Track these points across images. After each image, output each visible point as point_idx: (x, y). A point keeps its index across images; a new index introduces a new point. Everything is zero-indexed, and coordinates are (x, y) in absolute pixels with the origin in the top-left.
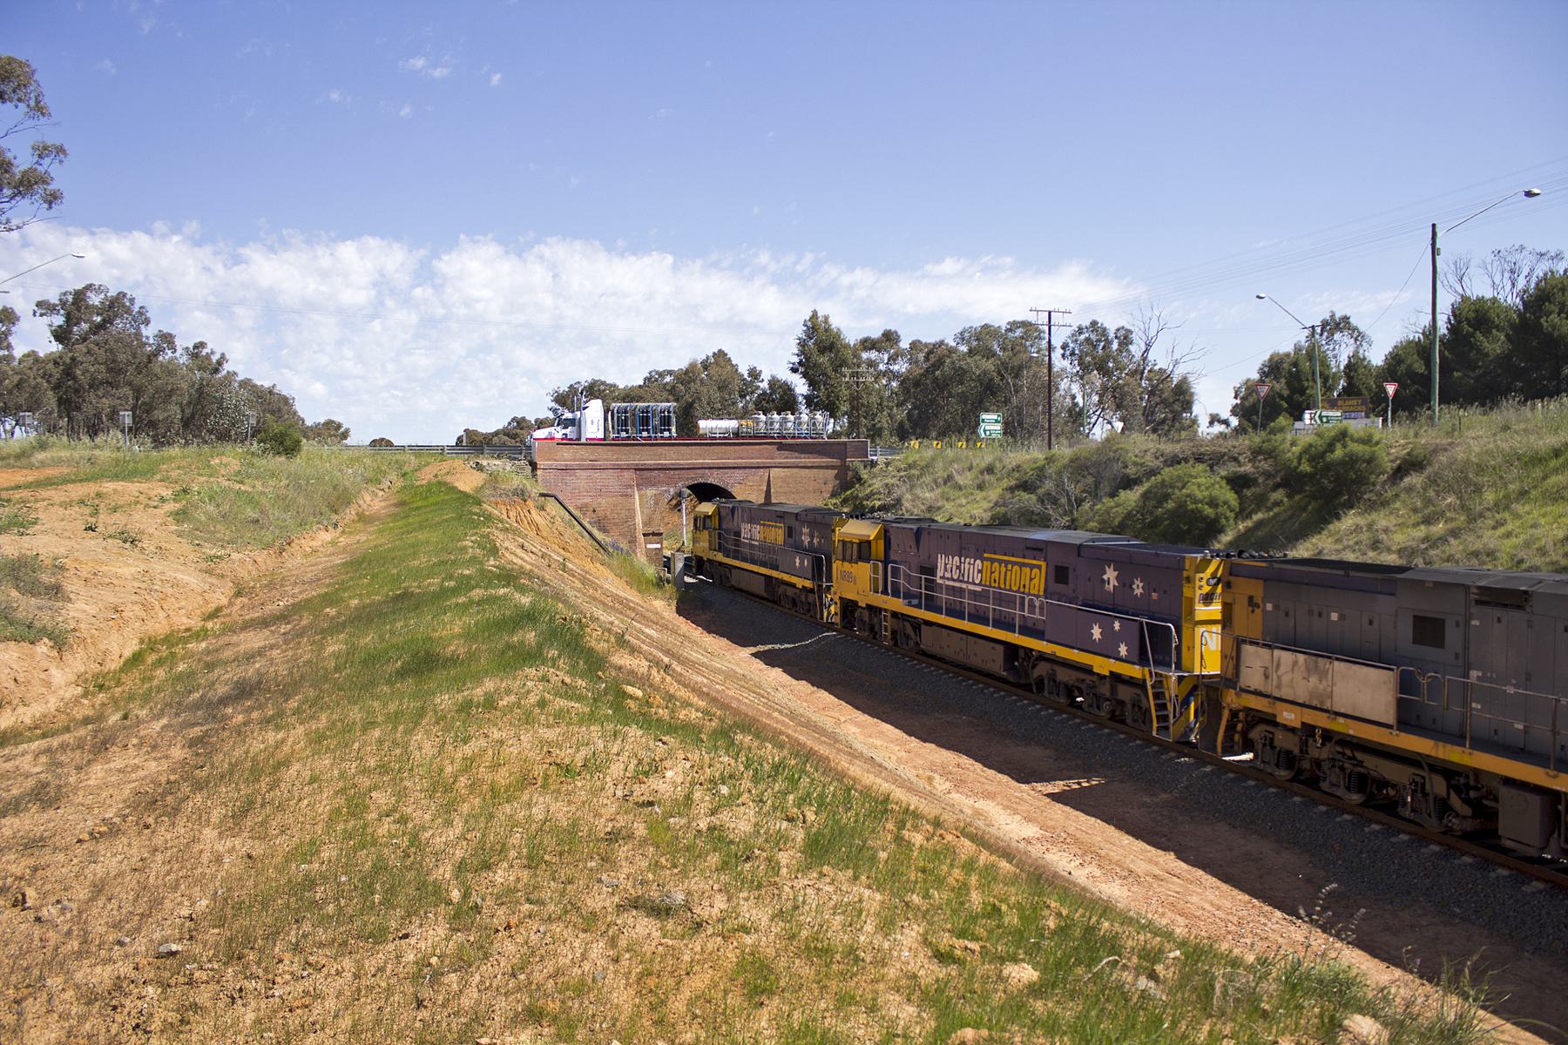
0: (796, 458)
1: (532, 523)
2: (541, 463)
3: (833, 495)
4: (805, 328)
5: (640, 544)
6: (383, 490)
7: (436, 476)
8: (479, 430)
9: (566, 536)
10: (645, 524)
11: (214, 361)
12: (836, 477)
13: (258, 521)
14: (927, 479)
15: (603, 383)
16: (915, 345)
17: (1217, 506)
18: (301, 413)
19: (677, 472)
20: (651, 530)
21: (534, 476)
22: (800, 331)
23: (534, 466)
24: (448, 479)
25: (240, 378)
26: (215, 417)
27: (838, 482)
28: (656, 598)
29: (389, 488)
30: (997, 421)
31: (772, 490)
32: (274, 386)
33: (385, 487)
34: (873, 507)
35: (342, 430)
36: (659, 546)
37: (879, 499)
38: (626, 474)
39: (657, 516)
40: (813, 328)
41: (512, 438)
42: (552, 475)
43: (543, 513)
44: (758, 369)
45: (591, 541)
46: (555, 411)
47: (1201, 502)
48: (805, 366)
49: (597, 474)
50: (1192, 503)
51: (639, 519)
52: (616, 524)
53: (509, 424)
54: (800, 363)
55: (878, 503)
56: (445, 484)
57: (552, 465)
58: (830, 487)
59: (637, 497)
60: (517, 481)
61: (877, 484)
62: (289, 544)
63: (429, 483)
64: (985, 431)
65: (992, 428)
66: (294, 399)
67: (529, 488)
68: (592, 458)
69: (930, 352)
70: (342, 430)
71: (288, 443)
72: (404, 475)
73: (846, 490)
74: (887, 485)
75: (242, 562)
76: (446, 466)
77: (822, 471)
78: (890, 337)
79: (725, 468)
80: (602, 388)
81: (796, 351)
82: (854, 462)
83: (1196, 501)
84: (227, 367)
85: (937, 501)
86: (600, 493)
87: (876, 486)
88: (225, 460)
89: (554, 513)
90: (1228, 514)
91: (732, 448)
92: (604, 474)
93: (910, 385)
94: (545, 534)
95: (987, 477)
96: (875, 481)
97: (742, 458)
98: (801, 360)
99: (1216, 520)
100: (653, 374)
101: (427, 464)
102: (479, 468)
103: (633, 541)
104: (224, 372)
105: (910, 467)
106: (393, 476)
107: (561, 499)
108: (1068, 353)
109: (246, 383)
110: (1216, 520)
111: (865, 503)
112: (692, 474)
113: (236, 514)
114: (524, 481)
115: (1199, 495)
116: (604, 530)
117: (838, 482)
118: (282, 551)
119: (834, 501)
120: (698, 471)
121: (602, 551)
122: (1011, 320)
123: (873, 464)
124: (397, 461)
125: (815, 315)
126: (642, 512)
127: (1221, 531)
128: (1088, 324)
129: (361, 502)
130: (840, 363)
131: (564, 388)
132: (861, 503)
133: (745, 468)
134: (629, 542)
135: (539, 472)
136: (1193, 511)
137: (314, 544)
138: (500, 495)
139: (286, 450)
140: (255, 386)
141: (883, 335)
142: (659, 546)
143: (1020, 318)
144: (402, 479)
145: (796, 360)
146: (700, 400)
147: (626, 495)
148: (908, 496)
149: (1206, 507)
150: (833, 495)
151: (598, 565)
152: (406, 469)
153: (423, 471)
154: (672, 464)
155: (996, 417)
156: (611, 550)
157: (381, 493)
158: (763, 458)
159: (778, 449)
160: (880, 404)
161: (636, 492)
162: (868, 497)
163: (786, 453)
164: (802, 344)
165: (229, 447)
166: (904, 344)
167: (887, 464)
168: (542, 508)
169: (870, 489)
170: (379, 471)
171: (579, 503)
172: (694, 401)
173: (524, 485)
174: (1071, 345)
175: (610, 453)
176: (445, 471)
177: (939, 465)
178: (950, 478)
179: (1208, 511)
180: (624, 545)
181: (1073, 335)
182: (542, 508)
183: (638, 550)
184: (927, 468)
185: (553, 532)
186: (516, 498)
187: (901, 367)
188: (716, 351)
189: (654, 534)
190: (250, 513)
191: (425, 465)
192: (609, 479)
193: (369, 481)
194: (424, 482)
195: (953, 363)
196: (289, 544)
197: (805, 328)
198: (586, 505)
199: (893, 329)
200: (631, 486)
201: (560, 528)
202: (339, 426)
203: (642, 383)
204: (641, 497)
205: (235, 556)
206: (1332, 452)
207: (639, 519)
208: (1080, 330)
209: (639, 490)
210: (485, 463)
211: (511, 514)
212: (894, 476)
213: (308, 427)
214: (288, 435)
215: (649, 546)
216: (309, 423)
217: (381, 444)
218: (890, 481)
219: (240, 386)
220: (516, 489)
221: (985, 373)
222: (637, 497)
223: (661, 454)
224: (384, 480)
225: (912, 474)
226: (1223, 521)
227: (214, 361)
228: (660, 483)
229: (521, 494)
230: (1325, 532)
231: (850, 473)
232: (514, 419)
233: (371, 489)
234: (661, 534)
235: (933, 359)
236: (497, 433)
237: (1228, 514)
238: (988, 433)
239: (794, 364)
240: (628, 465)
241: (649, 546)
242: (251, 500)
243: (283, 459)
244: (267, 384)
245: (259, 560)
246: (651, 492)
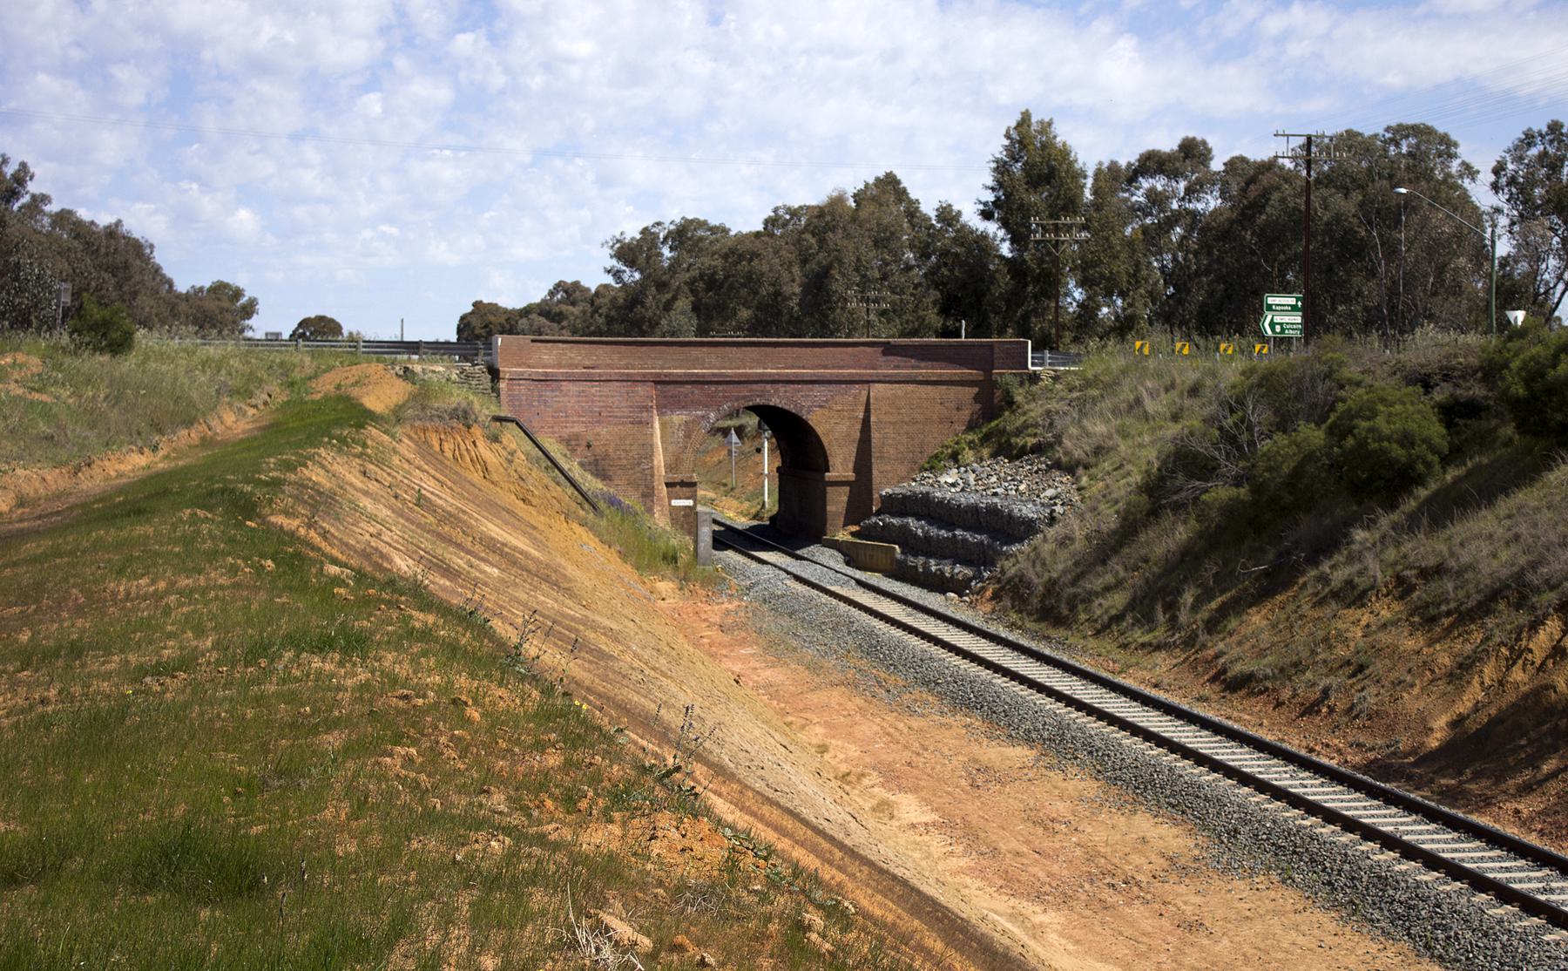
0: (913, 367)
1: (478, 461)
2: (506, 370)
3: (971, 427)
4: (1007, 142)
5: (660, 499)
6: (255, 406)
7: (338, 387)
8: (500, 304)
9: (530, 481)
10: (670, 468)
11: (8, 176)
12: (976, 398)
13: (52, 437)
14: (1107, 404)
15: (702, 224)
16: (1235, 165)
17: (1413, 444)
18: (168, 271)
19: (720, 388)
20: (678, 477)
21: (495, 389)
22: (997, 146)
23: (494, 373)
24: (355, 392)
25: (53, 208)
26: (8, 293)
27: (978, 406)
28: (663, 578)
29: (266, 403)
30: (1294, 308)
31: (873, 419)
32: (119, 223)
33: (260, 402)
34: (1024, 446)
35: (243, 300)
36: (690, 503)
37: (1035, 435)
38: (640, 389)
39: (689, 456)
40: (1020, 142)
41: (553, 320)
42: (522, 389)
43: (496, 446)
44: (956, 208)
45: (570, 490)
46: (617, 274)
47: (1389, 439)
48: (1004, 207)
49: (595, 389)
50: (1375, 441)
51: (659, 460)
52: (622, 467)
53: (551, 294)
54: (996, 203)
55: (1031, 441)
56: (348, 399)
57: (522, 373)
58: (966, 414)
59: (657, 425)
60: (457, 397)
61: (1035, 411)
62: (89, 465)
63: (326, 398)
64: (1272, 324)
65: (1286, 319)
66: (152, 246)
67: (477, 406)
68: (587, 363)
69: (1252, 181)
70: (243, 300)
71: (115, 335)
72: (292, 384)
73: (990, 420)
74: (1048, 412)
75: (28, 479)
76: (355, 372)
77: (954, 389)
78: (1193, 152)
79: (799, 382)
80: (700, 233)
81: (990, 182)
82: (1005, 375)
83: (1381, 439)
84: (33, 187)
85: (1110, 437)
86: (599, 418)
87: (1033, 414)
88: (21, 358)
89: (513, 446)
90: (1430, 457)
91: (808, 350)
92: (607, 389)
93: (1212, 233)
94: (495, 477)
95: (1187, 402)
96: (1033, 405)
97: (825, 367)
98: (998, 199)
99: (1410, 466)
100: (781, 212)
101: (330, 368)
102: (408, 374)
103: (648, 495)
104: (26, 199)
105: (1088, 384)
106: (274, 386)
107: (525, 425)
108: (1503, 180)
109: (64, 217)
110: (1410, 466)
111: (1013, 440)
112: (744, 391)
113: (27, 429)
114: (471, 397)
115: (1386, 429)
116: (603, 475)
117: (978, 406)
118: (78, 470)
119: (970, 437)
120: (754, 387)
121: (587, 506)
122: (1393, 123)
123: (1035, 378)
124: (282, 364)
125: (1025, 120)
126: (665, 450)
127: (1420, 481)
128: (1545, 130)
129: (214, 423)
130: (1067, 203)
131: (632, 232)
132: (1008, 442)
133: (830, 382)
134: (644, 495)
135: (503, 385)
136: (1374, 451)
137: (122, 467)
138: (431, 418)
139: (109, 345)
140: (79, 223)
141: (1180, 146)
142: (690, 503)
143: (1410, 120)
144: (287, 392)
145: (990, 197)
146: (840, 262)
147: (641, 422)
148: (1074, 431)
149: (1395, 446)
150: (971, 427)
151: (575, 526)
152: (297, 375)
153: (321, 380)
154: (714, 375)
155: (1292, 301)
156: (602, 505)
157: (251, 411)
158: (860, 367)
159: (884, 353)
160: (1135, 275)
161: (657, 418)
162: (1018, 432)
163: (897, 360)
164: (1001, 169)
165: (25, 338)
166: (1217, 165)
167: (1056, 379)
168: (496, 439)
169: (1023, 419)
170: (252, 377)
171: (566, 432)
172: (830, 267)
173: (470, 404)
174: (1510, 166)
175: (616, 357)
176: (352, 380)
177: (1126, 385)
178: (1138, 401)
179: (1397, 452)
180: (631, 500)
181: (1516, 148)
182: (496, 439)
183: (657, 509)
184: (1111, 386)
185: (509, 475)
186: (454, 423)
187: (1210, 202)
188: (881, 174)
189: (683, 484)
190: (43, 428)
191: (325, 371)
192: (614, 396)
193: (233, 393)
194: (318, 397)
195: (1283, 200)
196: (89, 465)
197: (1007, 142)
198: (577, 437)
199: (1199, 138)
200: (648, 409)
201: (523, 471)
202: (238, 293)
203: (760, 227)
204: (663, 425)
205: (19, 472)
206: (1554, 366)
207: (659, 460)
208: (1529, 139)
209: (661, 414)
210: (418, 368)
211: (446, 446)
212: (1062, 399)
213: (179, 296)
214: (114, 324)
215: (675, 503)
216: (182, 286)
217: (318, 329)
218: (1053, 405)
219: (54, 224)
220: (456, 409)
221: (1338, 218)
222: (657, 425)
223: (697, 359)
224: (257, 392)
225: (1085, 396)
226: (1420, 467)
227: (8, 176)
228: (696, 404)
229: (464, 417)
230: (1538, 485)
231: (998, 393)
232: (560, 286)
233: (237, 404)
234: (693, 485)
235: (1254, 191)
236: (526, 312)
237: (1430, 457)
238: (1278, 329)
239: (985, 204)
240: (644, 375)
241: (675, 503)
242: (46, 412)
243: (106, 358)
244: (104, 220)
245: (48, 478)
246: (678, 418)
